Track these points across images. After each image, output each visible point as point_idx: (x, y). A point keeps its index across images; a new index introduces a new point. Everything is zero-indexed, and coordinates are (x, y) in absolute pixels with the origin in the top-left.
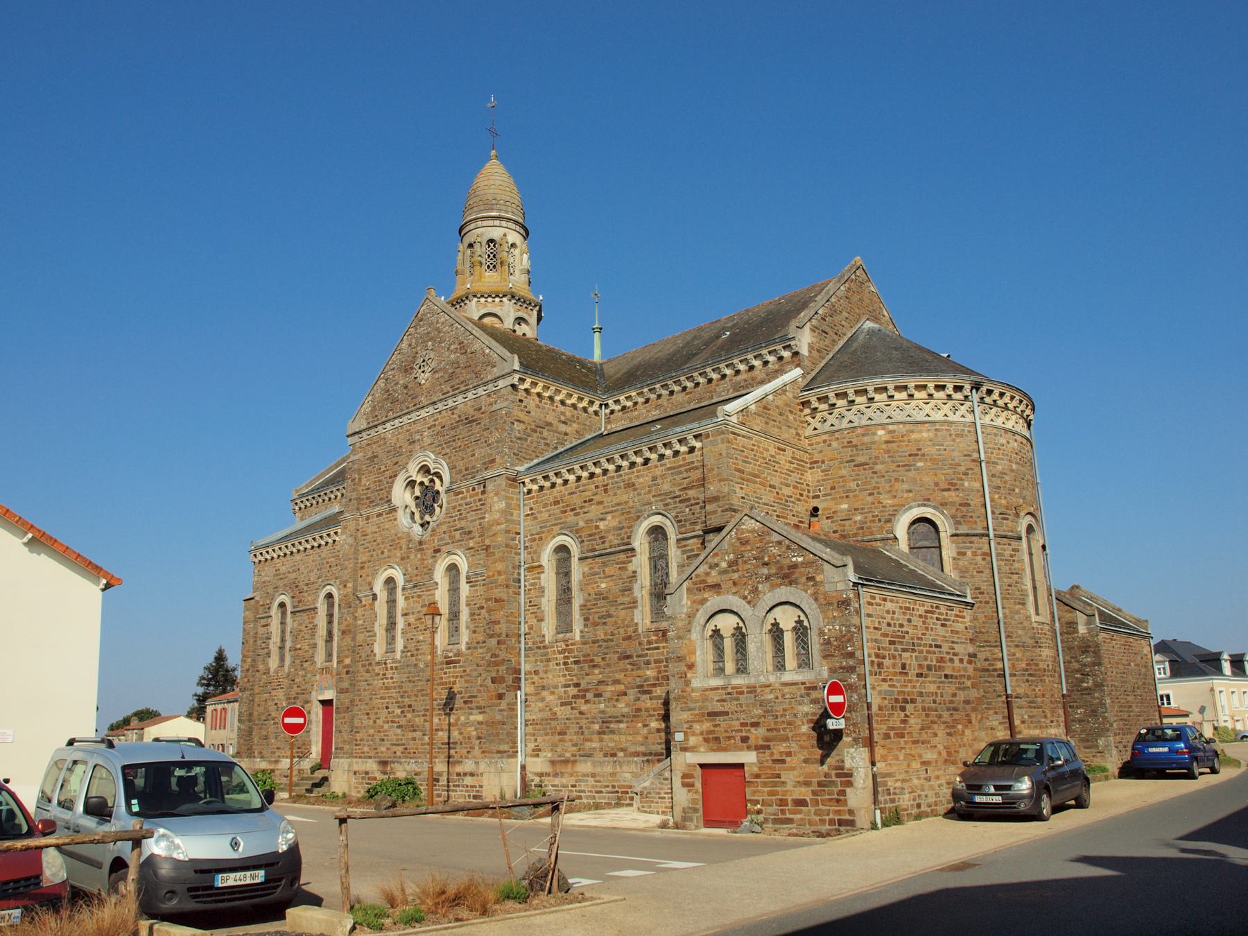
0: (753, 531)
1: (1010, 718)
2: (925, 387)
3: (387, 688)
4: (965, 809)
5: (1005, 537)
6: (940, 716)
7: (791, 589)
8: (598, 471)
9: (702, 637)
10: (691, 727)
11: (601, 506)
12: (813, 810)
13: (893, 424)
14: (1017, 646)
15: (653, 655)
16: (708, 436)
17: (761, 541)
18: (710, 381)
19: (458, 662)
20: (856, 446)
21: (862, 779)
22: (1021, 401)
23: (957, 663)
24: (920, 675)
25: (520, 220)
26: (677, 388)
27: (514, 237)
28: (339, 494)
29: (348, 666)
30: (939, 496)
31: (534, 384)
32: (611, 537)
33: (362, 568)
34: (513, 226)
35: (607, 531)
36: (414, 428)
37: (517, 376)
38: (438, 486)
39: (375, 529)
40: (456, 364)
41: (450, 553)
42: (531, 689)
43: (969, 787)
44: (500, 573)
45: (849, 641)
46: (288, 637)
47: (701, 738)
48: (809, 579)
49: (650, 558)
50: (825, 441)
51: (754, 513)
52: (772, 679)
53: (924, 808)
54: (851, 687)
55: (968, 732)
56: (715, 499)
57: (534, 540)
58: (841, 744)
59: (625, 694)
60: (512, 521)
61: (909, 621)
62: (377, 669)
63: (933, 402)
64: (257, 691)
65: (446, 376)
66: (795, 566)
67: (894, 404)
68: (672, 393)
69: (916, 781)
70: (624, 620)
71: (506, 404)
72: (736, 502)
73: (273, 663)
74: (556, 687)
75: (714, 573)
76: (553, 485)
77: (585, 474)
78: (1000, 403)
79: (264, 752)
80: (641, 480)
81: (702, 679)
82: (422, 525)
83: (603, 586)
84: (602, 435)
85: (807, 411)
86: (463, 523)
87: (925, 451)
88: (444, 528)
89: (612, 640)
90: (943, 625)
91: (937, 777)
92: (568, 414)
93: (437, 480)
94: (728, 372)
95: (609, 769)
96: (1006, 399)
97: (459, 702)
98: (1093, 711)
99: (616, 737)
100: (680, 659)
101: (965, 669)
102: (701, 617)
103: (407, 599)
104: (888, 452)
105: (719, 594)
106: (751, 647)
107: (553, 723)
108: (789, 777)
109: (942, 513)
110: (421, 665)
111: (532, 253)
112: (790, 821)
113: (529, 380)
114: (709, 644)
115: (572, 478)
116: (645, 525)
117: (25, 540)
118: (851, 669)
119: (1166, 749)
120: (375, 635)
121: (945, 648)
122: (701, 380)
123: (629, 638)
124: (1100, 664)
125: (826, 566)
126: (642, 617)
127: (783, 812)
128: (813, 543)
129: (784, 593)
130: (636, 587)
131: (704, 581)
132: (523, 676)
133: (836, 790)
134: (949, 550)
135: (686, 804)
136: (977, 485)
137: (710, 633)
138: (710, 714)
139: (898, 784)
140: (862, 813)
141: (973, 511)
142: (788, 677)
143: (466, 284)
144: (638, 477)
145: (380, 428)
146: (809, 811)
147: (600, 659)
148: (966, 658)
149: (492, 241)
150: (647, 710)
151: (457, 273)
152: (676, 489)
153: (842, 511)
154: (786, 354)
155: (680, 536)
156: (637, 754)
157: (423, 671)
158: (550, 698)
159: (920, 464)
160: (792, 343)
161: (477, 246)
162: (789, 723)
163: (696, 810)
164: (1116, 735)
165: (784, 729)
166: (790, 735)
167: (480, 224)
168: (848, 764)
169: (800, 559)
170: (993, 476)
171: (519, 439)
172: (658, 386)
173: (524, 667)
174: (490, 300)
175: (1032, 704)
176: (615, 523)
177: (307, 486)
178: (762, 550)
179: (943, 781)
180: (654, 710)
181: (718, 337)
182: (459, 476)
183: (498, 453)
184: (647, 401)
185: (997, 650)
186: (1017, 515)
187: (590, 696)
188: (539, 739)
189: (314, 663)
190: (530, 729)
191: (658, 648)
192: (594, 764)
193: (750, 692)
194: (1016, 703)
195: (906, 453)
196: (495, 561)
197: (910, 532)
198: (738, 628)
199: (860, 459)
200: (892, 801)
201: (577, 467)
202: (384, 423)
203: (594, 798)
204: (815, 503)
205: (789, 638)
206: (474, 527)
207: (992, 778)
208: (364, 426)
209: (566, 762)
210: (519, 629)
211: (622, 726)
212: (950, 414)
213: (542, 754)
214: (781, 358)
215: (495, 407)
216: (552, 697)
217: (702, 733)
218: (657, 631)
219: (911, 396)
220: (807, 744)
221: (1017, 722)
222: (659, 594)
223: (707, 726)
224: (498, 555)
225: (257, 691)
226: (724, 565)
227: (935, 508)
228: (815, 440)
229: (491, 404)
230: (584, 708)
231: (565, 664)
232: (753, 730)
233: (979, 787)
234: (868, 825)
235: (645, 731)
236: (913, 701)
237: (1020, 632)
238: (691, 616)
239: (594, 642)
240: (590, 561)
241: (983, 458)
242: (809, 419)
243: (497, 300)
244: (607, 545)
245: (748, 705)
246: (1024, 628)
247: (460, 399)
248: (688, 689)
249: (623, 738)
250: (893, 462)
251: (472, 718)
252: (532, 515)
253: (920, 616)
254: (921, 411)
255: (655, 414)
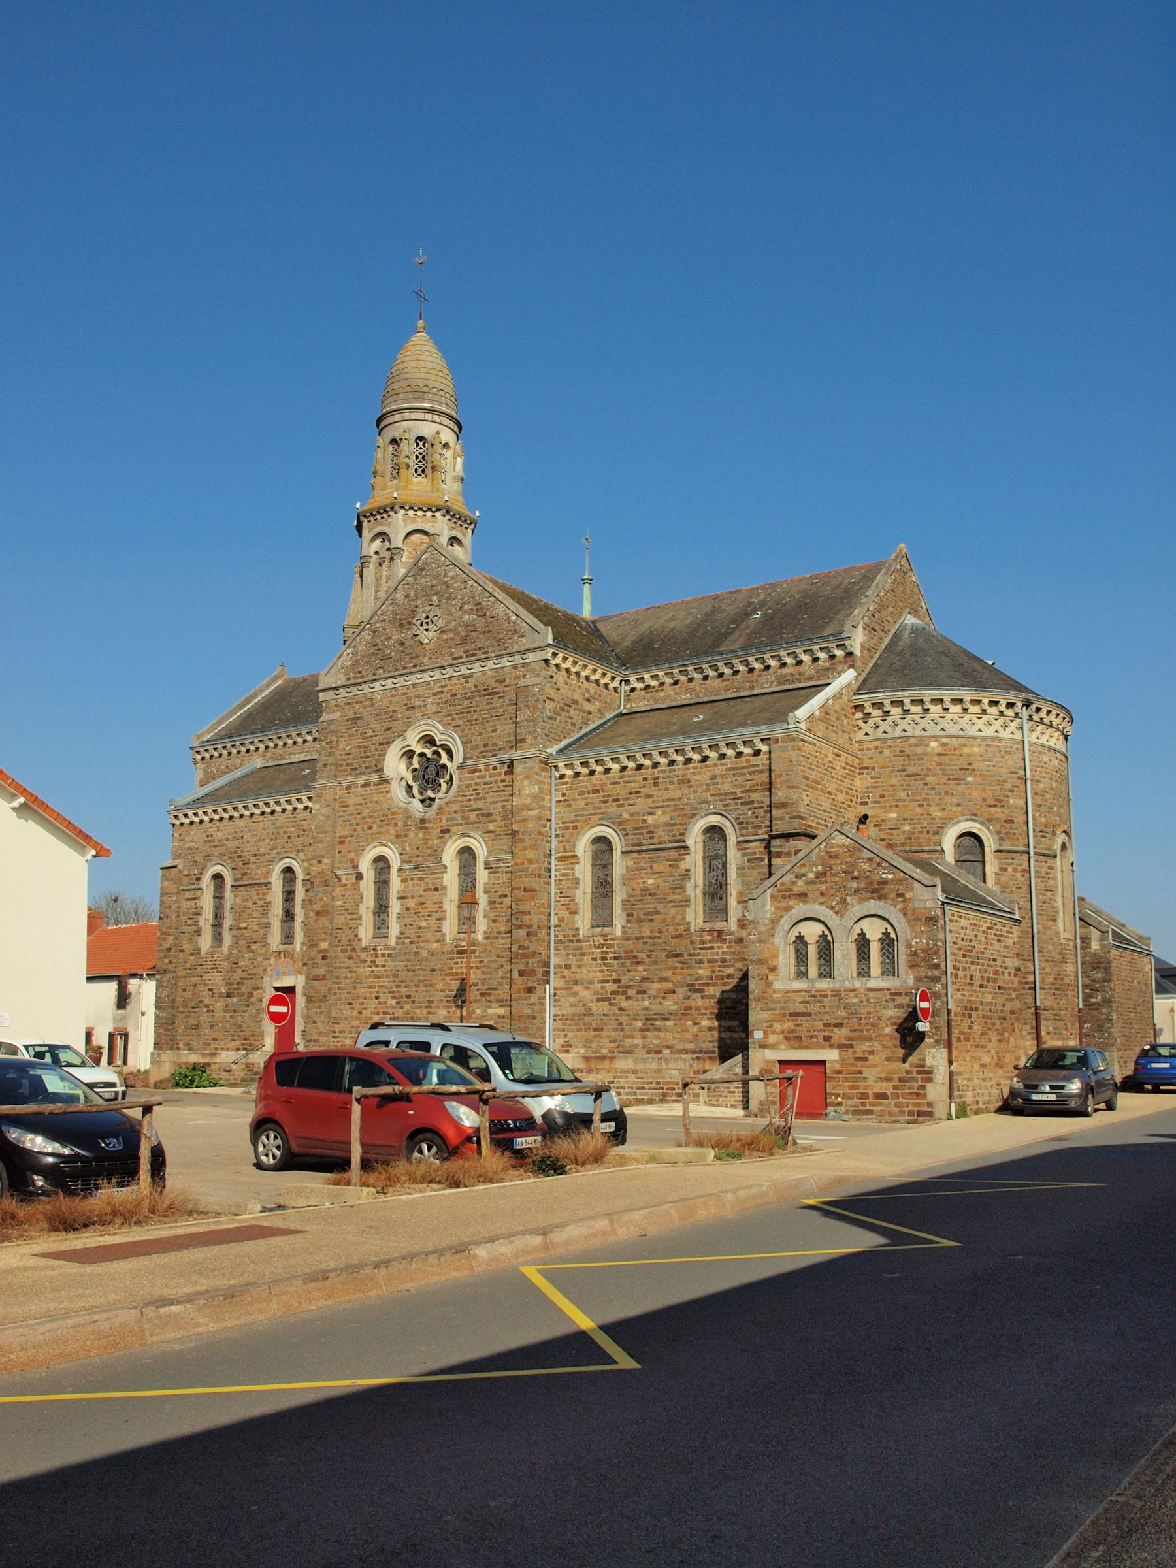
0: (842, 846)
1: (1037, 1029)
2: (979, 702)
3: (377, 977)
4: (1015, 1106)
5: (1043, 855)
6: (994, 1024)
7: (881, 903)
9: (786, 942)
10: (771, 1026)
11: (650, 800)
12: (893, 1102)
14: (1047, 961)
15: (706, 955)
16: (777, 741)
17: (851, 856)
18: (751, 670)
19: (474, 952)
21: (941, 1076)
22: (1058, 715)
23: (1006, 976)
24: (981, 986)
25: (454, 414)
26: (712, 673)
27: (447, 436)
29: (325, 950)
31: (565, 659)
33: (342, 843)
35: (657, 826)
37: (551, 651)
39: (359, 800)
41: (463, 835)
42: (562, 984)
43: (1026, 1086)
44: (530, 861)
45: (935, 953)
46: (227, 913)
47: (781, 1037)
48: (899, 895)
49: (704, 858)
50: (876, 748)
51: (846, 829)
52: (857, 984)
53: (981, 1105)
54: (936, 995)
55: (1012, 1040)
56: (783, 805)
57: (567, 828)
58: (922, 1045)
59: (674, 992)
60: (544, 807)
61: (976, 936)
62: (363, 956)
63: (985, 717)
64: (181, 973)
66: (885, 882)
68: (706, 678)
69: (976, 1081)
70: (674, 918)
73: (205, 942)
74: (592, 982)
75: (800, 882)
76: (592, 773)
78: (1046, 721)
79: (194, 1044)
80: (698, 777)
81: (784, 980)
82: (422, 801)
83: (651, 882)
84: (621, 715)
85: (859, 715)
86: (480, 804)
88: (455, 807)
89: (659, 938)
90: (999, 941)
91: (990, 1079)
92: (592, 691)
93: (443, 753)
94: (773, 663)
95: (654, 1065)
97: (473, 994)
99: (662, 1035)
100: (761, 962)
102: (785, 923)
103: (404, 881)
105: (805, 902)
106: (838, 955)
107: (587, 1019)
108: (870, 1074)
109: (988, 829)
110: (424, 954)
111: (467, 453)
112: (869, 1112)
113: (561, 655)
115: (615, 767)
116: (701, 824)
117: (16, 804)
118: (936, 979)
119: (1167, 1065)
120: (360, 918)
121: (999, 963)
122: (741, 668)
123: (680, 936)
124: (1109, 981)
125: (916, 884)
126: (695, 916)
127: (863, 1104)
128: (904, 863)
129: (873, 906)
130: (689, 886)
131: (790, 890)
132: (552, 970)
133: (916, 1085)
134: (991, 866)
135: (763, 1097)
136: (1021, 803)
137: (794, 939)
138: (790, 1015)
139: (965, 1082)
140: (940, 1105)
142: (873, 983)
144: (694, 773)
145: (365, 686)
147: (644, 956)
148: (1013, 971)
149: (421, 438)
150: (698, 1008)
151: (375, 473)
152: (738, 791)
153: (891, 820)
154: (839, 653)
156: (686, 1052)
157: (426, 959)
159: (970, 779)
160: (847, 643)
162: (873, 1025)
163: (774, 1103)
164: (1119, 1050)
165: (868, 1030)
167: (407, 415)
168: (929, 1062)
169: (890, 876)
170: (1036, 794)
171: (550, 718)
173: (553, 961)
174: (420, 513)
175: (1057, 1017)
176: (666, 819)
177: (209, 731)
178: (853, 865)
179: (993, 1083)
180: (706, 1009)
181: (748, 615)
182: (476, 752)
183: (529, 733)
184: (676, 683)
185: (1030, 964)
186: (1054, 833)
187: (631, 992)
188: (570, 1035)
189: (266, 945)
190: (559, 1024)
191: (712, 948)
192: (635, 1060)
194: (1044, 1014)
195: (955, 766)
196: (525, 849)
197: (957, 846)
198: (823, 936)
199: (912, 770)
200: (961, 1096)
201: (623, 757)
202: (372, 682)
203: (635, 1094)
204: (864, 810)
205: (875, 948)
207: (1044, 1079)
208: (342, 681)
209: (603, 1058)
210: (549, 921)
211: (668, 1023)
212: (1001, 730)
214: (833, 657)
215: (522, 683)
216: (586, 993)
217: (782, 1032)
218: (711, 932)
219: (966, 710)
221: (1043, 1033)
222: (716, 893)
223: (788, 1025)
226: (811, 876)
227: (982, 823)
228: (865, 746)
229: (518, 678)
230: (624, 1004)
231: (603, 959)
232: (836, 1030)
233: (1036, 1087)
234: (945, 1116)
235: (695, 1029)
236: (977, 1009)
237: (1050, 947)
238: (774, 922)
239: (637, 939)
240: (635, 855)
241: (1028, 776)
242: (860, 723)
243: (429, 514)
244: (656, 840)
245: (831, 1007)
246: (1053, 944)
247: (476, 667)
249: (669, 1036)
250: (944, 775)
251: (490, 1011)
254: (971, 724)
255: (685, 698)
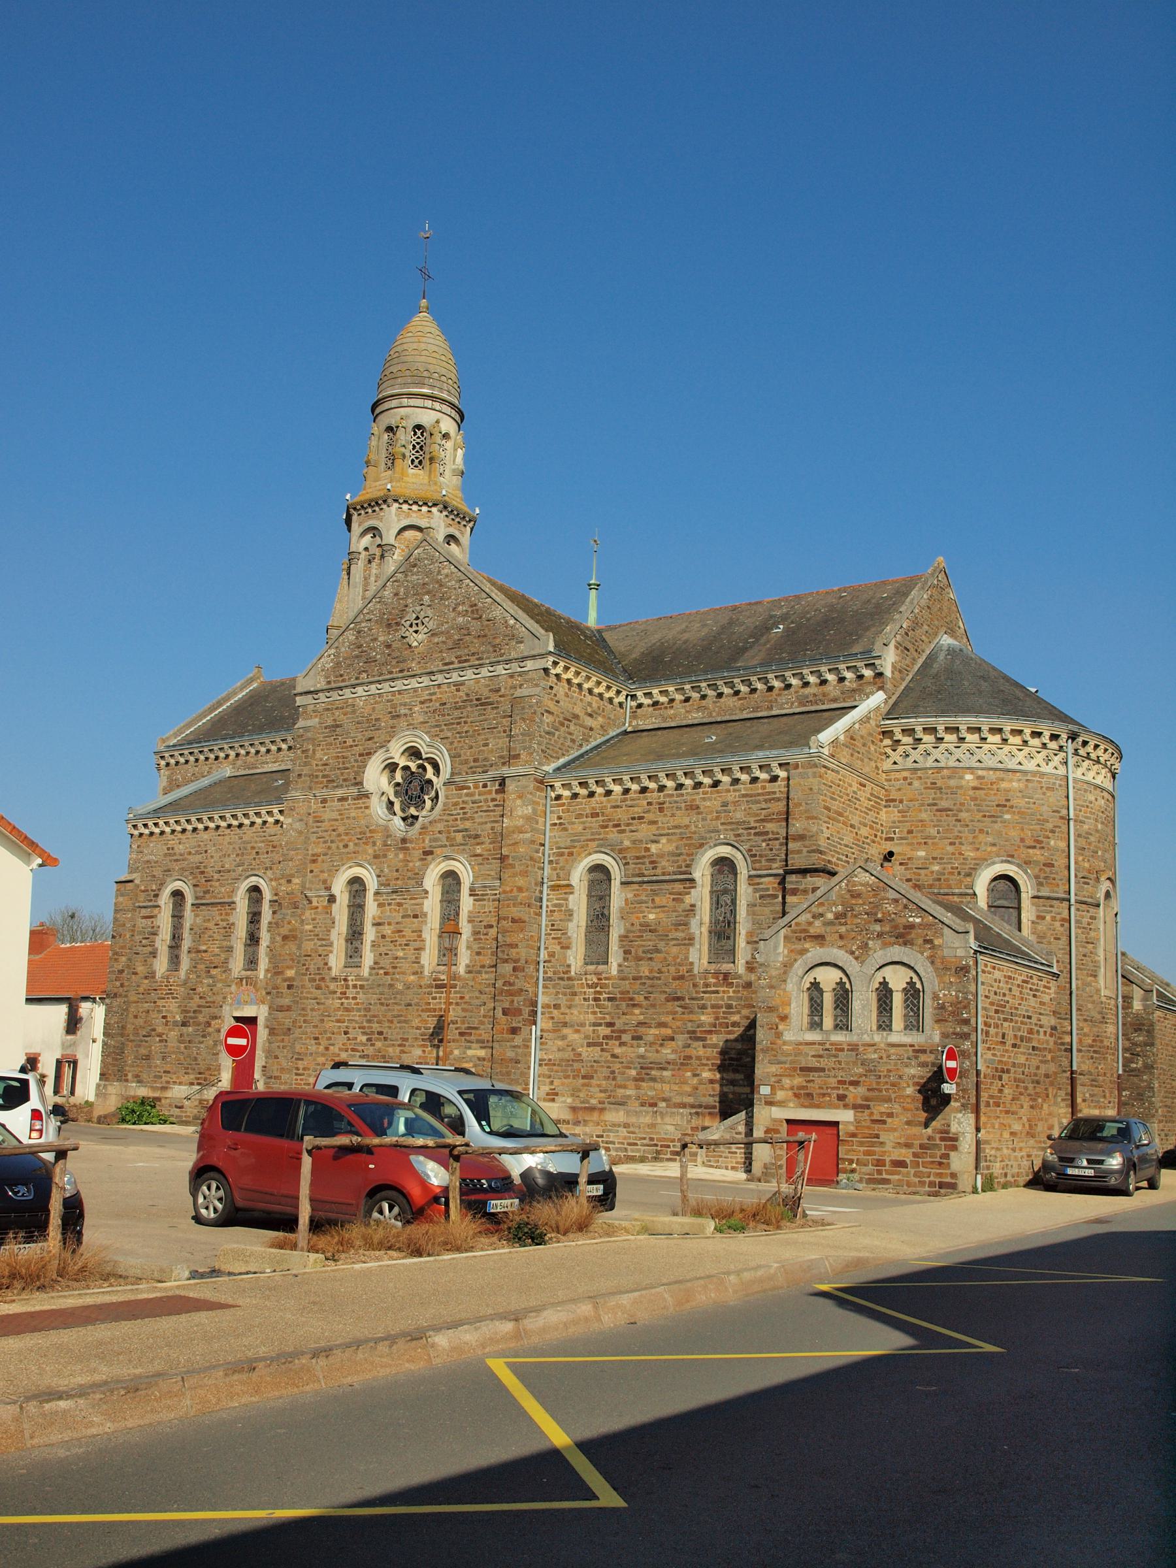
0: (867, 884)
2: (1020, 732)
3: (347, 1010)
6: (1026, 1088)
7: (907, 950)
8: (652, 785)
9: (799, 989)
10: (779, 1081)
11: (654, 827)
12: (912, 1171)
13: (982, 769)
14: (1086, 1020)
16: (796, 766)
17: (875, 896)
18: (771, 689)
19: (455, 986)
20: (941, 788)
21: (967, 1144)
22: (1106, 750)
24: (1014, 1046)
27: (448, 425)
28: (232, 754)
30: (1024, 853)
31: (566, 669)
32: (664, 863)
33: (314, 861)
34: (448, 410)
35: (661, 856)
36: (398, 699)
37: (551, 659)
38: (430, 773)
39: (335, 815)
40: (464, 630)
41: (448, 858)
42: (549, 1025)
43: (1061, 1159)
44: (520, 889)
45: (965, 1007)
47: (790, 1093)
48: (926, 941)
49: (711, 892)
50: (905, 779)
52: (877, 1038)
53: (1009, 1178)
54: (964, 1054)
55: (1045, 1106)
56: (801, 837)
57: (562, 854)
59: (672, 1039)
61: (1010, 990)
63: (1027, 750)
64: (133, 998)
65: (450, 644)
66: (912, 926)
67: (986, 747)
68: (720, 695)
69: (1005, 1151)
70: (675, 958)
71: (537, 690)
72: (823, 843)
73: (161, 965)
74: (583, 1025)
75: (817, 923)
76: (592, 794)
77: (635, 787)
78: (1093, 756)
79: (144, 1076)
81: (796, 1031)
83: (652, 916)
84: (625, 733)
85: (887, 742)
86: (468, 824)
87: (1014, 802)
88: (440, 826)
90: (1034, 996)
91: (1021, 1149)
92: (595, 705)
93: (429, 768)
94: (794, 682)
96: (1100, 752)
97: (451, 1033)
98: (1138, 1094)
99: (658, 1086)
100: (771, 1009)
101: (1047, 1042)
102: (799, 967)
103: (380, 905)
104: (974, 799)
105: (822, 945)
106: (856, 1005)
107: (576, 1065)
109: (1026, 873)
111: (468, 445)
113: (562, 664)
114: (805, 997)
115: (617, 789)
116: (710, 854)
118: (966, 1036)
120: (331, 945)
123: (682, 977)
124: (1152, 1045)
125: (946, 930)
126: (699, 956)
129: (897, 952)
130: (694, 923)
133: (939, 1153)
134: (1028, 913)
136: (1063, 845)
137: (808, 985)
138: (802, 1069)
139: (993, 1152)
140: (966, 1176)
141: (1057, 873)
142: (894, 1038)
143: (380, 482)
144: (704, 799)
146: (908, 1173)
147: (642, 998)
148: (1049, 1030)
150: (699, 1058)
151: (368, 463)
152: (752, 819)
153: (919, 858)
154: (868, 673)
155: (753, 873)
156: (684, 1105)
157: (401, 993)
158: (573, 1037)
159: (1007, 817)
160: (877, 662)
161: (400, 433)
162: (893, 1085)
164: (1160, 1122)
165: (887, 1090)
166: (893, 1096)
167: (405, 401)
168: (954, 1128)
169: (918, 920)
171: (548, 733)
172: (704, 685)
173: (542, 999)
174: (415, 508)
175: (1094, 1083)
176: (671, 848)
177: (176, 735)
178: (877, 906)
180: (708, 1059)
181: (768, 629)
182: (465, 768)
184: (687, 700)
185: (1067, 1023)
186: (1098, 880)
187: (626, 1038)
189: (227, 970)
191: (717, 992)
192: (628, 1113)
193: (852, 1050)
194: (1080, 1079)
196: (515, 875)
197: (991, 890)
198: (841, 984)
199: (944, 804)
201: (626, 778)
202: (354, 686)
204: (889, 846)
205: (898, 1000)
206: (485, 831)
208: (322, 685)
209: (592, 1109)
210: (538, 955)
211: (665, 1073)
212: (1043, 764)
213: (559, 1099)
214: (861, 677)
216: (576, 1036)
217: (792, 1088)
218: (716, 974)
219: (1005, 740)
220: (912, 1106)
221: (1079, 1100)
222: (723, 932)
223: (798, 1081)
224: (518, 869)
225: (133, 998)
226: (830, 916)
227: (1019, 866)
228: (893, 776)
230: (618, 1051)
231: (596, 999)
232: (851, 1088)
233: (1072, 1160)
234: (970, 1189)
235: (695, 1081)
236: (1008, 1071)
237: (1090, 1006)
238: (787, 966)
239: (635, 979)
240: (636, 886)
241: (1072, 816)
242: (889, 750)
243: (425, 509)
244: (659, 871)
245: (847, 1063)
246: (1093, 1002)
247: (469, 674)
248: (779, 1042)
249: (666, 1087)
250: (979, 811)
251: (470, 1052)
252: (560, 825)
253: (1019, 986)
254: (1014, 756)
255: (697, 717)
